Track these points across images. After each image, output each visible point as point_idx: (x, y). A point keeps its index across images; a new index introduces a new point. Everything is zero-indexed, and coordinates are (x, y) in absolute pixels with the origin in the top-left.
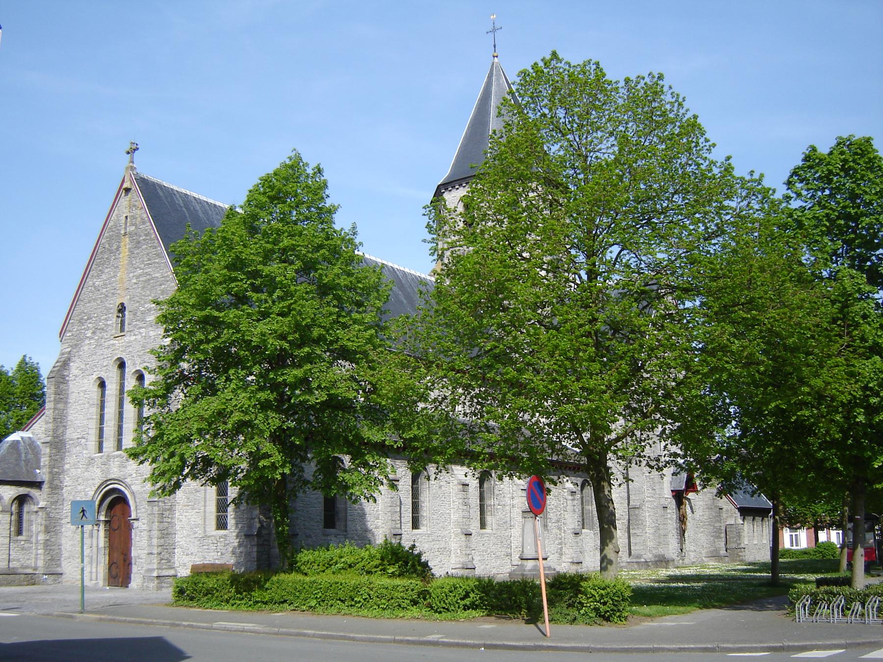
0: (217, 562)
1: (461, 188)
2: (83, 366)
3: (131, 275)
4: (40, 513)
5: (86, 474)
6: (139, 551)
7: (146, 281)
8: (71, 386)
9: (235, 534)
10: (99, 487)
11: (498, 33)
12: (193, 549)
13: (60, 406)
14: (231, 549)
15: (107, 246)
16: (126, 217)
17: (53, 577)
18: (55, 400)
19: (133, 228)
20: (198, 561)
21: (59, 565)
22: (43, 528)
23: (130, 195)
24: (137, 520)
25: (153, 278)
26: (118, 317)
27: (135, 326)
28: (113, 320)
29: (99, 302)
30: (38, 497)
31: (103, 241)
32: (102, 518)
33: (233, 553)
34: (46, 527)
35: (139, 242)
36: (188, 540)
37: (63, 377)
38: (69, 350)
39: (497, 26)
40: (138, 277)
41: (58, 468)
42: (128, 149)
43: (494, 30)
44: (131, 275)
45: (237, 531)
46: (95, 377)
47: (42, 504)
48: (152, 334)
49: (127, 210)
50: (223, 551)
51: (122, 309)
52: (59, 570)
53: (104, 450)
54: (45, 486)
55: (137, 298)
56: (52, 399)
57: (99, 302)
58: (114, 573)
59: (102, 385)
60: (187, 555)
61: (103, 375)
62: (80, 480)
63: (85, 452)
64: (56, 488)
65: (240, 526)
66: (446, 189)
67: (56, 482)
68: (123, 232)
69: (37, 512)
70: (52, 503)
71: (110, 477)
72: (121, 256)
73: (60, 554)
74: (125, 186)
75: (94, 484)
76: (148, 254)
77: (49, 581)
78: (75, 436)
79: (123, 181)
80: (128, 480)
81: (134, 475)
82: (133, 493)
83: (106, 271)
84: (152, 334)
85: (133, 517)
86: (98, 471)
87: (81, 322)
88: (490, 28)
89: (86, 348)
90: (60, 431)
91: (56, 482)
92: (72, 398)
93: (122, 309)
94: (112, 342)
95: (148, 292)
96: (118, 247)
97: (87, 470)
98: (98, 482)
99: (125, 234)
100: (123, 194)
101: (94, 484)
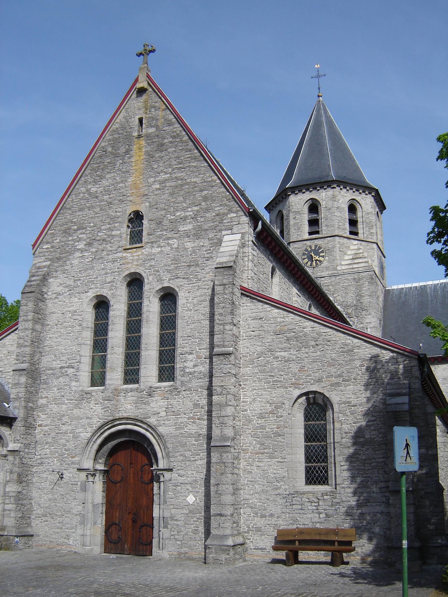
0: (318, 526)
1: (308, 192)
2: (71, 283)
3: (152, 180)
4: (10, 458)
5: (75, 411)
6: (173, 511)
7: (176, 187)
8: (50, 305)
9: (351, 490)
10: (100, 428)
11: (321, 79)
12: (276, 510)
13: (38, 327)
14: (343, 510)
15: (110, 149)
16: (141, 120)
17: (23, 540)
18: (33, 319)
19: (152, 130)
20: (284, 525)
21: (29, 525)
22: (15, 476)
23: (144, 97)
24: (170, 470)
25: (188, 184)
26: (128, 227)
27: (159, 237)
28: (124, 231)
29: (97, 210)
30: (8, 437)
31: (103, 144)
32: (101, 467)
33: (348, 514)
34: (19, 475)
35: (162, 145)
36: (263, 497)
37: (42, 293)
38: (48, 263)
39: (321, 73)
40: (161, 183)
41: (33, 402)
42: (141, 50)
43: (318, 76)
44: (152, 180)
45: (354, 486)
46: (91, 294)
47: (12, 446)
48: (189, 245)
49: (141, 112)
50: (331, 512)
51: (137, 218)
52: (30, 531)
53: (107, 382)
54: (18, 424)
55: (162, 206)
56: (30, 317)
57: (97, 210)
58: (114, 536)
59: (102, 305)
60: (263, 516)
61: (105, 292)
62: (65, 419)
63: (74, 384)
64: (29, 427)
65: (359, 480)
66: (293, 192)
67: (30, 420)
68: (135, 134)
69: (5, 456)
70: (27, 446)
71: (117, 416)
72: (133, 159)
73: (30, 510)
74: (138, 85)
75: (90, 425)
76: (178, 158)
77: (21, 546)
78: (56, 364)
79: (137, 81)
80: (152, 421)
81: (163, 414)
82: (160, 436)
83: (108, 176)
84: (189, 245)
85: (161, 466)
86: (98, 409)
87: (67, 232)
88: (315, 74)
89: (76, 262)
90: (36, 358)
91: (30, 420)
92: (51, 320)
93: (137, 218)
94: (120, 255)
95: (181, 199)
96: (127, 152)
97: (77, 406)
98: (96, 422)
99: (139, 137)
100: (134, 95)
101: (90, 425)
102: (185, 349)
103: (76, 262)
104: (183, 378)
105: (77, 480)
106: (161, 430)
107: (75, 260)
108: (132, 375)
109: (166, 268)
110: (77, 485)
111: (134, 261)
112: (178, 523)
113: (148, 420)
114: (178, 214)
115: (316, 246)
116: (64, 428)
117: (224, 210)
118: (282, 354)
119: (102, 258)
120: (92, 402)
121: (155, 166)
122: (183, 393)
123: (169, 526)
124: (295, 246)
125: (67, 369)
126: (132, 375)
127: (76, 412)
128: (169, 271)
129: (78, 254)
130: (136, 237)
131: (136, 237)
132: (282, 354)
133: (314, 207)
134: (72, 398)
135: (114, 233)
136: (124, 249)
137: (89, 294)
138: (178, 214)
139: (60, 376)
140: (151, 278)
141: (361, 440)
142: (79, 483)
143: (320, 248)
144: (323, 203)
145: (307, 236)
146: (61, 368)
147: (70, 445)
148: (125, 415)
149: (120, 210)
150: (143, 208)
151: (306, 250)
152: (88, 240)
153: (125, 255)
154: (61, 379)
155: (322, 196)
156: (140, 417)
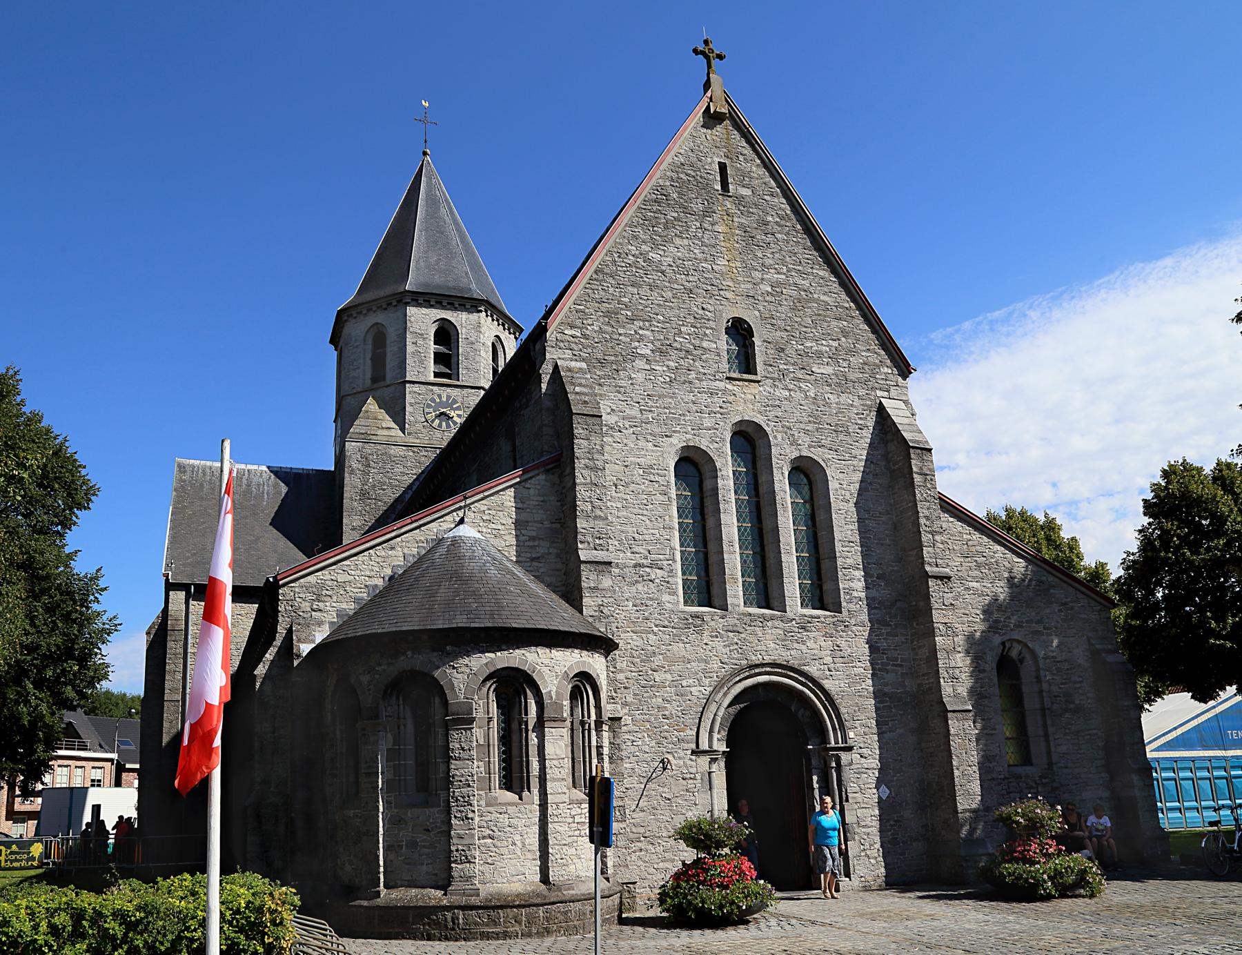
62: (658, 661)
80: (813, 670)
81: (828, 660)
93: (740, 331)
94: (721, 385)
102: (848, 561)
103: (639, 377)
104: (851, 606)
105: (693, 770)
106: (827, 684)
107: (638, 372)
108: (766, 591)
109: (802, 426)
110: (694, 779)
111: (747, 402)
112: (869, 830)
113: (806, 668)
114: (808, 344)
115: (448, 397)
116: (658, 677)
117: (874, 359)
118: (974, 584)
119: (690, 383)
120: (706, 633)
121: (760, 255)
122: (854, 628)
123: (857, 837)
124: (416, 389)
125: (648, 570)
126: (766, 591)
127: (678, 648)
128: (806, 432)
129: (640, 364)
130: (746, 362)
131: (746, 362)
132: (974, 584)
133: (446, 334)
134: (666, 623)
135: (705, 344)
136: (728, 378)
137: (674, 440)
138: (808, 344)
139: (637, 582)
140: (779, 436)
141: (1072, 706)
142: (698, 776)
143: (455, 401)
144: (463, 332)
145: (431, 378)
146: (635, 566)
147: (672, 709)
148: (768, 659)
149: (712, 309)
150: (751, 317)
151: (433, 400)
152: (658, 344)
153: (729, 387)
154: (640, 586)
155: (460, 319)
156: (794, 663)
